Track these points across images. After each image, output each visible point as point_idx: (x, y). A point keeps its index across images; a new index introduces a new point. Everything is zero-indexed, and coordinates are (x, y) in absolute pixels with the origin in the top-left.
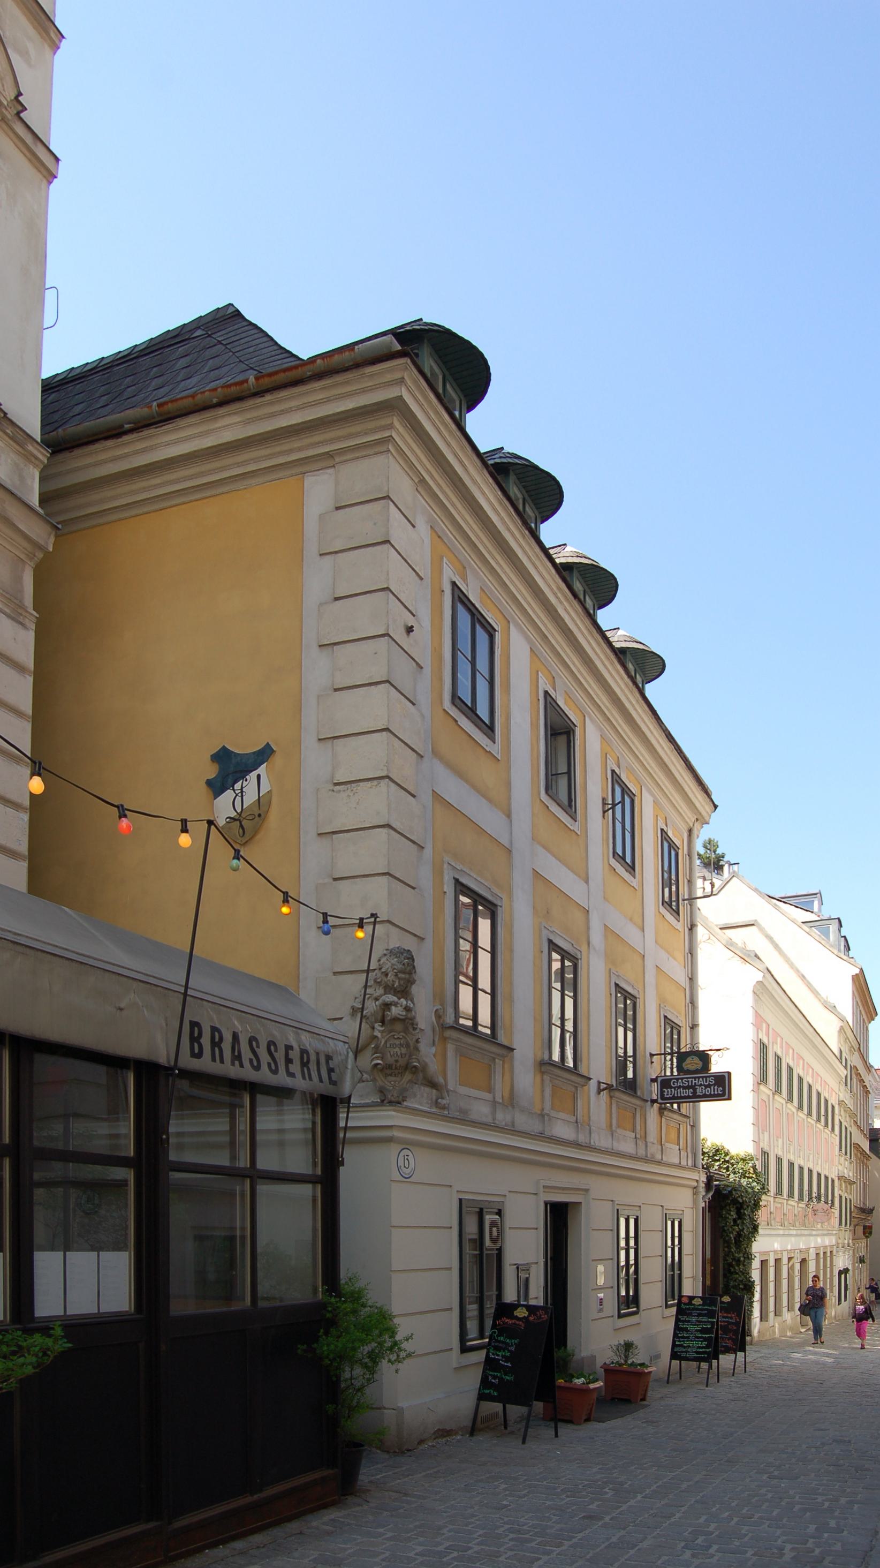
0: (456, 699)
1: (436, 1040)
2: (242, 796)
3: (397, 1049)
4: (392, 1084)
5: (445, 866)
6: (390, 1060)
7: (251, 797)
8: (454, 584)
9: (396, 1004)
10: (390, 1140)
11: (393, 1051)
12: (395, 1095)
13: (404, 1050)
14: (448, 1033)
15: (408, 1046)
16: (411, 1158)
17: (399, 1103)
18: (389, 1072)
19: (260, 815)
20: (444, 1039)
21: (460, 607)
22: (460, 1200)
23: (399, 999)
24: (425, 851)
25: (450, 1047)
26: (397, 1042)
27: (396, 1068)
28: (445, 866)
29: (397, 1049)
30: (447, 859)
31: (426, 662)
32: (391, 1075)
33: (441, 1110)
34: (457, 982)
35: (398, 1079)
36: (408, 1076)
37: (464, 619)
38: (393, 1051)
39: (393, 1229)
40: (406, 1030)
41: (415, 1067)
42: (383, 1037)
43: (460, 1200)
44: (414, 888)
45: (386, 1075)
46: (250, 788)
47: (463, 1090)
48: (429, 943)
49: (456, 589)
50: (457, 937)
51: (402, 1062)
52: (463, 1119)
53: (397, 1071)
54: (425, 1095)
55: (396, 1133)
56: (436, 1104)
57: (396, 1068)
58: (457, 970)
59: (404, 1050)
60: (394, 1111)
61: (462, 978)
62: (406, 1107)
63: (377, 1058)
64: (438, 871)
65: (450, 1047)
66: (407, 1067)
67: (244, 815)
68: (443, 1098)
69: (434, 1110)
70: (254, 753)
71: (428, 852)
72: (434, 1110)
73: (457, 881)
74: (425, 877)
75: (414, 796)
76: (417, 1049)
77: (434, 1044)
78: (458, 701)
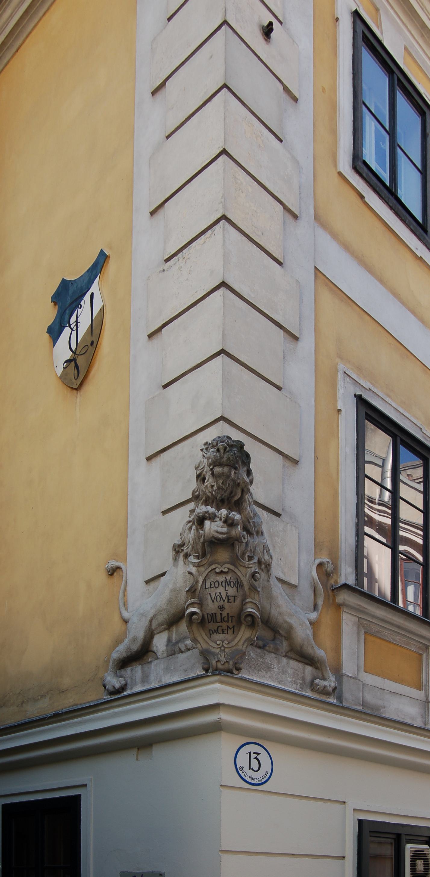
0: (360, 165)
1: (320, 602)
2: (77, 330)
3: (221, 590)
4: (219, 643)
5: (340, 375)
6: (211, 607)
7: (84, 328)
8: (356, 14)
9: (212, 518)
10: (217, 728)
11: (214, 592)
12: (223, 659)
13: (232, 591)
14: (344, 597)
15: (238, 584)
16: (264, 757)
17: (231, 672)
18: (212, 626)
19: (92, 343)
20: (339, 607)
21: (367, 57)
22: (360, 822)
23: (218, 509)
24: (300, 344)
25: (348, 622)
26: (221, 578)
27: (222, 620)
28: (340, 375)
29: (221, 590)
30: (341, 367)
31: (306, 92)
32: (217, 631)
33: (331, 698)
34: (360, 536)
35: (229, 636)
36: (244, 633)
37: (376, 80)
38: (214, 592)
39: (224, 857)
40: (235, 561)
41: (250, 615)
42: (200, 574)
43: (360, 822)
44: (279, 388)
45: (211, 633)
46: (83, 317)
47: (370, 679)
48: (306, 469)
49: (359, 22)
50: (361, 477)
51: (231, 609)
52: (370, 714)
53: (224, 625)
54: (290, 671)
55: (225, 716)
56: (312, 686)
57: (222, 620)
58: (362, 520)
59: (232, 591)
60: (221, 682)
61: (367, 530)
62: (242, 679)
63: (192, 604)
64: (325, 379)
65: (348, 622)
66: (241, 619)
67: (78, 353)
68: (324, 679)
69: (309, 694)
70: (88, 271)
71: (307, 343)
72: (309, 694)
73: (360, 400)
74: (300, 375)
75: (280, 263)
76: (253, 588)
77: (315, 608)
78: (360, 164)
